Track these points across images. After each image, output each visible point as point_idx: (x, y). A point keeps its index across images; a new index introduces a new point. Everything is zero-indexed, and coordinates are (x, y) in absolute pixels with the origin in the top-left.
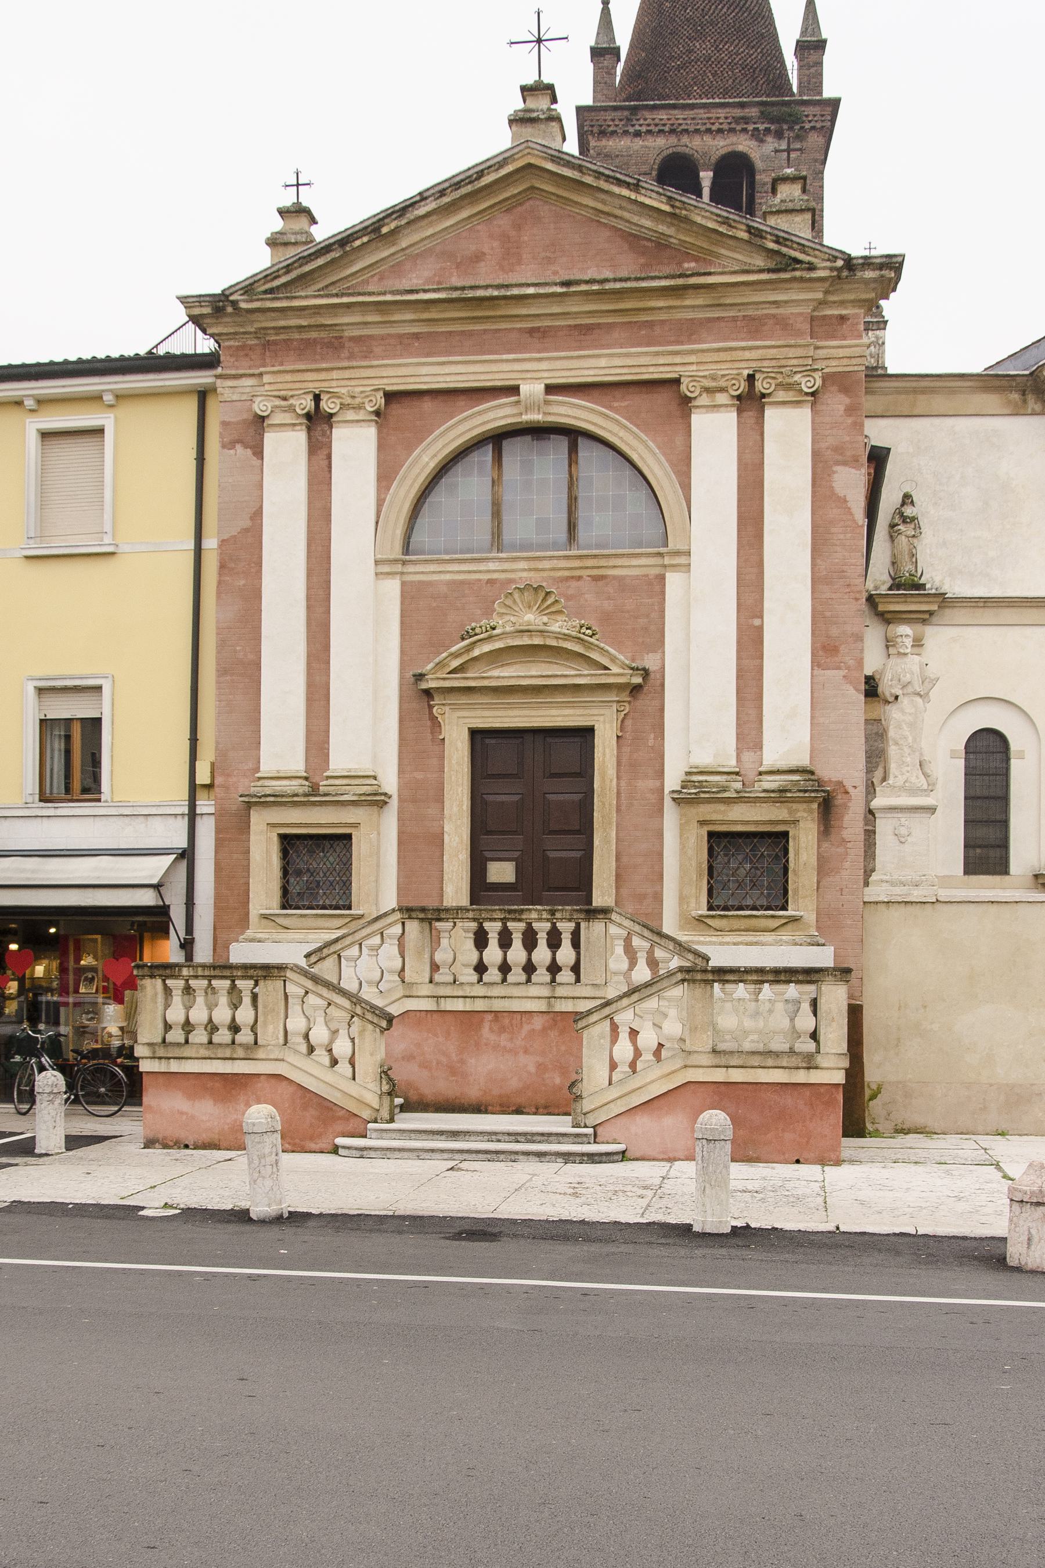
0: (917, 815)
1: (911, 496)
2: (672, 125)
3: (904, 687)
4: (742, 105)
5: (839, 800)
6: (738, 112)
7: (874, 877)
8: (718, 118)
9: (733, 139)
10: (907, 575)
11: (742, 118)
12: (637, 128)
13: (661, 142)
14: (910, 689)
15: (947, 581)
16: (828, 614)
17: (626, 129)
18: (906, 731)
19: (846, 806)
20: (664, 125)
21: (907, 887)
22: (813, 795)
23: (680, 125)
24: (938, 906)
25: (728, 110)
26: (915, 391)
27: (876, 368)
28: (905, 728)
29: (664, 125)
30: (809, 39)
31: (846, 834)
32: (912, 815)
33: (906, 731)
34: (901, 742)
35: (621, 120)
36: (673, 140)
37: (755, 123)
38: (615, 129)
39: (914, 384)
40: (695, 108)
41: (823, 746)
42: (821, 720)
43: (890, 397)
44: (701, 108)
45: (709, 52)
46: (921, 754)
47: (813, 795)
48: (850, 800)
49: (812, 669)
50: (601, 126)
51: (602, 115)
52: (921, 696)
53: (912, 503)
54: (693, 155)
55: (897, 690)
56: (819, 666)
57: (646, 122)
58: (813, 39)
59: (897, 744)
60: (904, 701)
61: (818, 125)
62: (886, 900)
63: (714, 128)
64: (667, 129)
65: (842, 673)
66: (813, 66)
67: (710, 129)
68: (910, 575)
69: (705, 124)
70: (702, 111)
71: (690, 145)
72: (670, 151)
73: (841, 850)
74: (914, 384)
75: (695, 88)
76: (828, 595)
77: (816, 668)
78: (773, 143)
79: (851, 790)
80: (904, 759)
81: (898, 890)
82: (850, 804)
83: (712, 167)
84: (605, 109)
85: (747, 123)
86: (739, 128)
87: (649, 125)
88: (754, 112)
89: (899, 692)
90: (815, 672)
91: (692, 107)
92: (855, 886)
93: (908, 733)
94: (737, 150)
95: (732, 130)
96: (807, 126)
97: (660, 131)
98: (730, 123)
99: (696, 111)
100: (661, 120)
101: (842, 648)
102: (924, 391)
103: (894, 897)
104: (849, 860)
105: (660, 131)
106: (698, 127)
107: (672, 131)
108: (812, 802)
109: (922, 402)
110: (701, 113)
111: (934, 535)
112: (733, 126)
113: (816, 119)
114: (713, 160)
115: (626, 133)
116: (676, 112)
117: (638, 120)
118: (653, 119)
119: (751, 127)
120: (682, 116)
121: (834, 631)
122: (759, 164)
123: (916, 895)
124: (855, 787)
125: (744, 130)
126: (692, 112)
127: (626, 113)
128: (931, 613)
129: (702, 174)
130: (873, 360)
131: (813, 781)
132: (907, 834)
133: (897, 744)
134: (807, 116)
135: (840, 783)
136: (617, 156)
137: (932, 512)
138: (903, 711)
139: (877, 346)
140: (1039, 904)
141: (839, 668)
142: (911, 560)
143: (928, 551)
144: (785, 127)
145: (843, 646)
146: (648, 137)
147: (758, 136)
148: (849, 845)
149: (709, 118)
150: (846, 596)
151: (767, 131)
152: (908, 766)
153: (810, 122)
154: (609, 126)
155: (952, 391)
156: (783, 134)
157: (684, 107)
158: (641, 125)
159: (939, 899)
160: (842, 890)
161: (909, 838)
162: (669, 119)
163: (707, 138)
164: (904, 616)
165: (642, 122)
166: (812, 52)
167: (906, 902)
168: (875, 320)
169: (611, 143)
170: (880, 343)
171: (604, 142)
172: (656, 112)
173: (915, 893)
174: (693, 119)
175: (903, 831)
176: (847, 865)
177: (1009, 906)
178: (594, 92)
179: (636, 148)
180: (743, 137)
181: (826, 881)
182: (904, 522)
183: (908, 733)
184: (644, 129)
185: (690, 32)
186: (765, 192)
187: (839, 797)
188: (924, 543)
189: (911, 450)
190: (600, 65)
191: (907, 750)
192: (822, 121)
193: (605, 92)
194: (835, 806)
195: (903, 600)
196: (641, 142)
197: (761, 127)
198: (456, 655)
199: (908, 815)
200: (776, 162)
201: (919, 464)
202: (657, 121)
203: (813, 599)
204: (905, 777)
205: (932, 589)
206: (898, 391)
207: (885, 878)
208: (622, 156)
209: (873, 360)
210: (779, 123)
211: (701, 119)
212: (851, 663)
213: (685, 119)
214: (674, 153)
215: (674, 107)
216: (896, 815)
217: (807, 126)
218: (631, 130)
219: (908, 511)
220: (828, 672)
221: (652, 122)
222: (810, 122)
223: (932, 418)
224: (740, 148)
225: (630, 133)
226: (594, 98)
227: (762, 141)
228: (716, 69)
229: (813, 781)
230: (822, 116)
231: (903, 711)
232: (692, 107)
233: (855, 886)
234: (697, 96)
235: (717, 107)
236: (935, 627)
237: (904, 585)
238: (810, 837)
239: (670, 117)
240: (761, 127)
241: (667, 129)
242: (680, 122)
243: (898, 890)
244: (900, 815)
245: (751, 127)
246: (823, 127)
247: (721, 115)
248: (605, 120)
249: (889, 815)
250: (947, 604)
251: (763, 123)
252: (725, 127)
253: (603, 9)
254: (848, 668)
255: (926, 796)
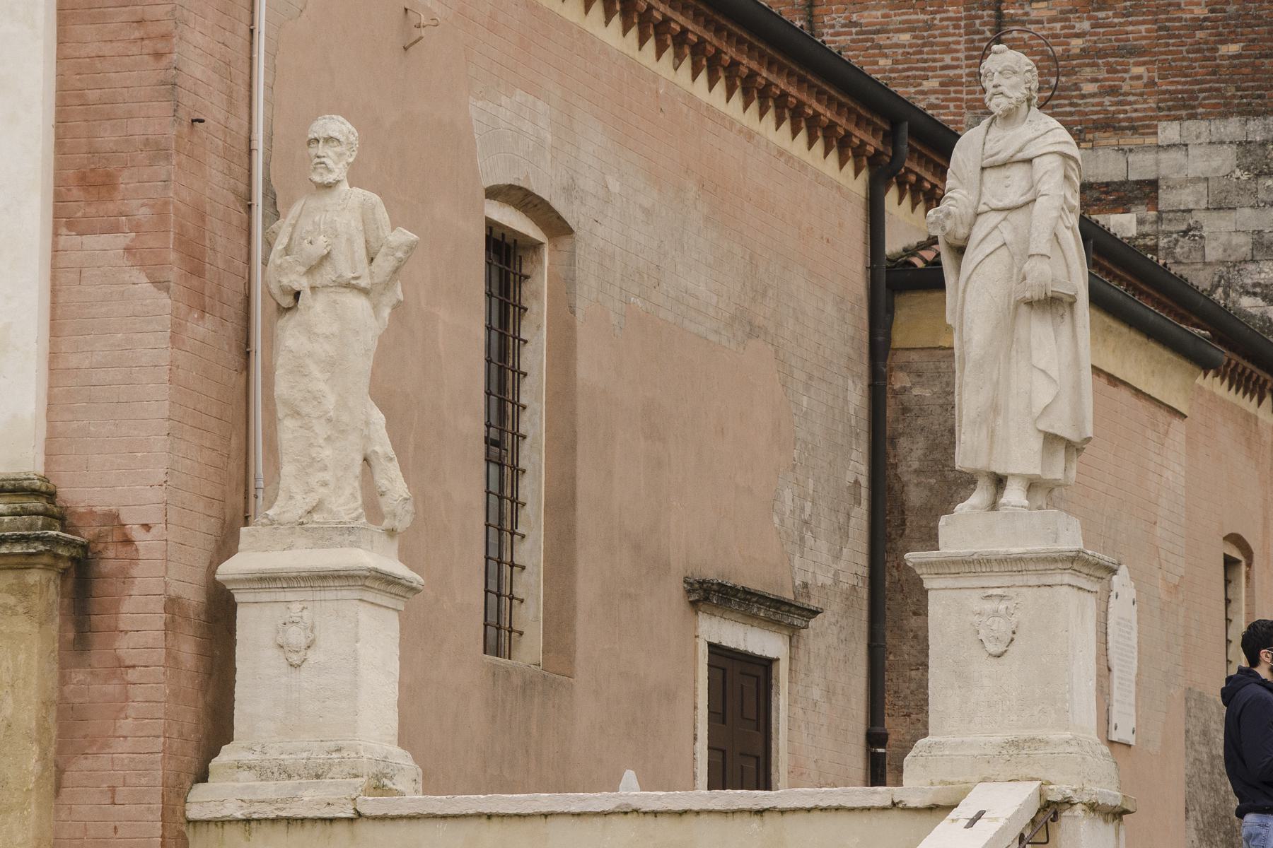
0: (330, 595)
3: (311, 270)
5: (111, 560)
7: (227, 755)
14: (327, 275)
16: (92, 95)
18: (319, 381)
19: (125, 576)
21: (294, 782)
22: (18, 549)
24: (362, 828)
28: (319, 375)
31: (126, 647)
32: (319, 595)
33: (319, 381)
34: (306, 409)
41: (75, 425)
42: (74, 361)
46: (367, 439)
47: (18, 549)
48: (135, 560)
49: (56, 234)
52: (365, 292)
55: (293, 277)
56: (70, 225)
59: (296, 413)
60: (316, 308)
62: (239, 815)
65: (122, 240)
73: (113, 688)
76: (92, 49)
77: (64, 231)
79: (137, 534)
80: (314, 453)
81: (270, 789)
82: (134, 572)
89: (302, 283)
90: (62, 239)
92: (144, 781)
93: (322, 386)
101: (126, 181)
103: (256, 807)
104: (131, 712)
108: (28, 567)
121: (107, 138)
123: (310, 800)
124: (147, 527)
131: (31, 513)
132: (303, 642)
133: (296, 413)
135: (113, 519)
138: (310, 333)
140: (599, 821)
141: (114, 229)
145: (126, 173)
148: (132, 675)
150: (134, 49)
152: (325, 468)
159: (362, 810)
160: (113, 789)
161: (310, 652)
167: (290, 821)
173: (308, 795)
175: (296, 636)
176: (126, 725)
177: (528, 825)
181: (78, 769)
183: (322, 386)
187: (110, 553)
191: (321, 429)
194: (103, 576)
198: (1126, 112)
199: (307, 595)
203: (61, 58)
204: (312, 500)
207: (246, 757)
212: (143, 214)
216: (281, 596)
220: (90, 241)
229: (31, 513)
231: (310, 333)
233: (144, 781)
238: (22, 657)
243: (270, 789)
244: (290, 596)
249: (264, 597)
254: (137, 229)
255: (352, 544)
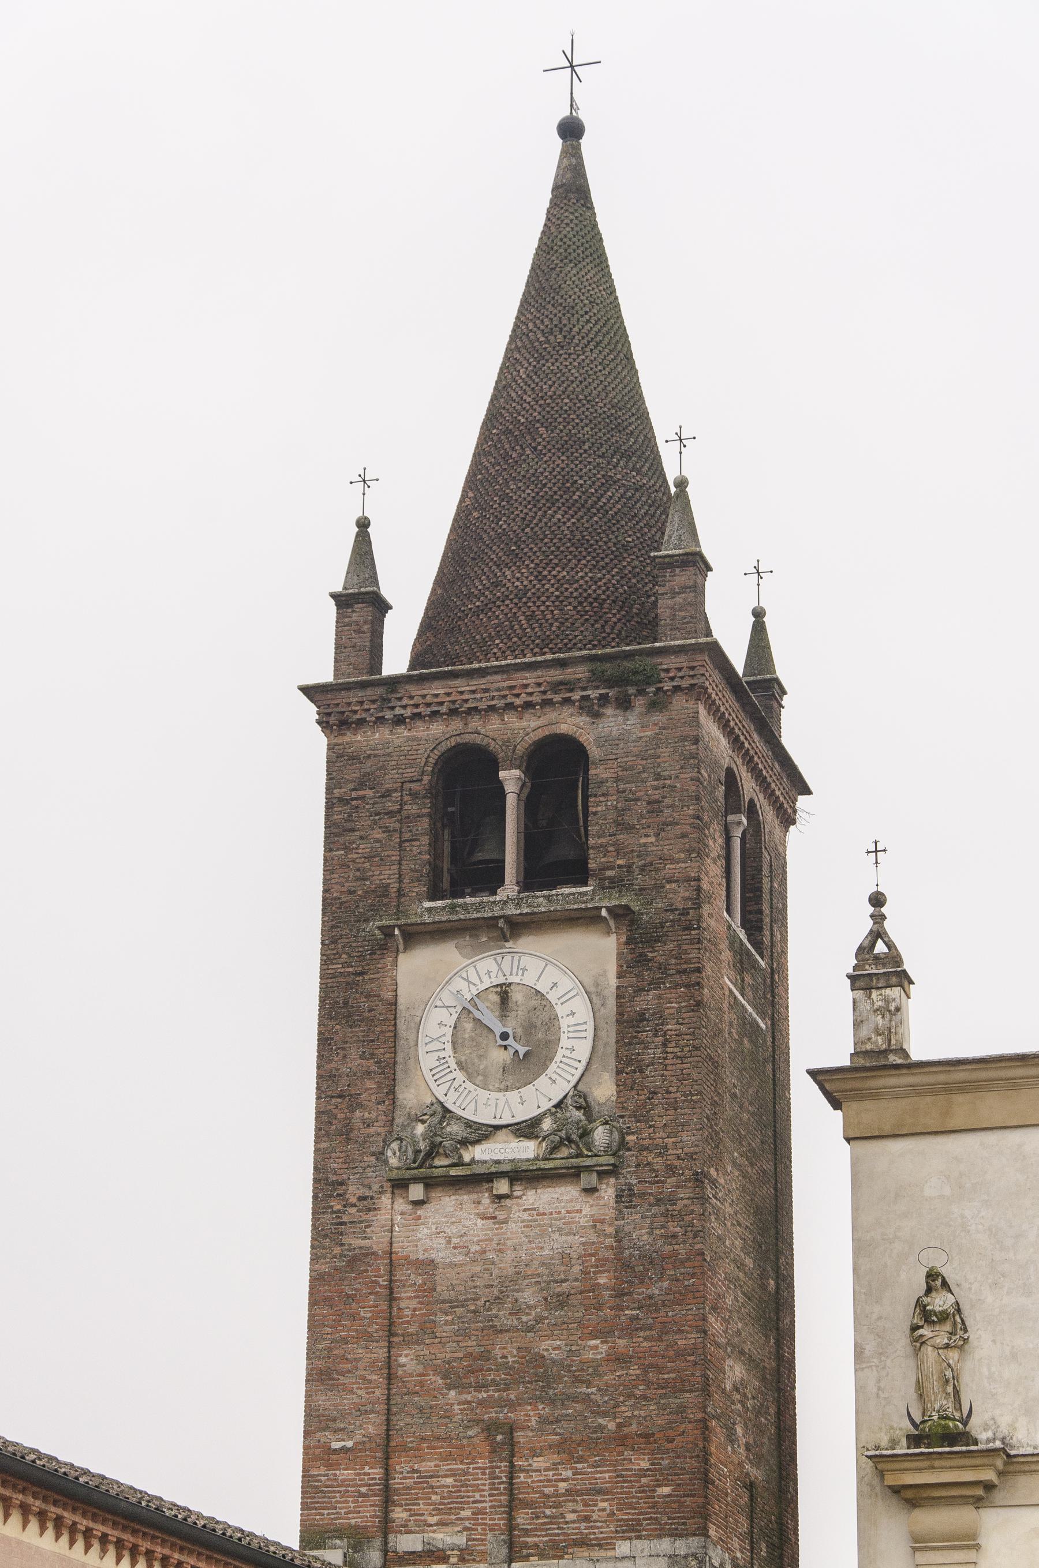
1: (938, 1274)
2: (454, 702)
4: (562, 664)
6: (556, 675)
8: (526, 686)
9: (551, 715)
10: (935, 1418)
11: (561, 683)
12: (398, 711)
13: (437, 729)
15: (1022, 1423)
17: (381, 714)
20: (441, 704)
23: (466, 701)
25: (539, 673)
26: (947, 1089)
27: (884, 1053)
29: (441, 704)
30: (670, 552)
35: (373, 702)
36: (456, 725)
37: (584, 689)
38: (364, 715)
39: (942, 1078)
40: (488, 674)
43: (904, 1102)
44: (496, 673)
45: (525, 583)
50: (343, 713)
51: (344, 697)
53: (945, 1284)
54: (488, 744)
57: (412, 702)
58: (677, 552)
61: (685, 683)
63: (518, 701)
64: (444, 709)
66: (679, 593)
67: (512, 703)
68: (941, 1418)
69: (505, 696)
70: (498, 677)
71: (482, 731)
72: (453, 742)
74: (942, 1078)
75: (497, 641)
78: (614, 716)
83: (518, 762)
84: (347, 687)
85: (571, 690)
86: (557, 698)
87: (416, 706)
88: (581, 672)
91: (483, 672)
94: (558, 732)
95: (547, 703)
96: (667, 686)
97: (435, 714)
98: (544, 692)
99: (489, 678)
100: (436, 696)
102: (963, 1088)
105: (435, 714)
106: (493, 703)
107: (453, 712)
109: (962, 1108)
110: (497, 681)
111: (994, 1341)
112: (549, 696)
113: (680, 674)
114: (520, 750)
115: (381, 720)
116: (457, 682)
117: (400, 699)
118: (424, 696)
119: (576, 696)
120: (468, 688)
122: (594, 752)
125: (567, 701)
126: (483, 681)
127: (380, 691)
128: (989, 1487)
129: (502, 774)
130: (880, 1040)
134: (667, 671)
136: (369, 756)
137: (990, 1299)
139: (887, 1015)
142: (944, 1390)
143: (985, 1370)
144: (631, 690)
146: (419, 723)
147: (592, 710)
149: (511, 688)
151: (604, 699)
153: (672, 679)
154: (355, 712)
155: (1014, 1085)
156: (630, 702)
157: (470, 674)
158: (404, 707)
162: (448, 694)
163: (510, 718)
164: (937, 1493)
165: (405, 702)
166: (677, 570)
168: (882, 971)
169: (359, 738)
170: (892, 1008)
171: (348, 737)
172: (428, 685)
174: (487, 690)
178: (336, 661)
179: (397, 742)
180: (567, 711)
182: (928, 1321)
184: (408, 712)
185: (500, 554)
186: (603, 795)
188: (977, 1357)
189: (947, 1191)
190: (347, 620)
192: (692, 676)
193: (352, 660)
195: (926, 1464)
196: (406, 733)
197: (593, 694)
198: (594, 1533)
200: (621, 746)
201: (963, 1216)
202: (429, 699)
205: (994, 1440)
206: (919, 1091)
208: (375, 756)
209: (880, 1040)
210: (621, 686)
211: (498, 690)
213: (473, 692)
214: (458, 745)
215: (454, 675)
217: (667, 686)
218: (389, 715)
219: (940, 1302)
221: (421, 701)
222: (672, 679)
223: (982, 1134)
224: (564, 729)
225: (387, 720)
226: (336, 670)
227: (597, 715)
228: (535, 609)
230: (693, 668)
232: (483, 672)
234: (499, 654)
235: (523, 669)
236: (999, 1510)
237: (928, 1436)
239: (450, 691)
240: (593, 694)
241: (444, 709)
242: (465, 697)
245: (576, 696)
246: (693, 685)
247: (529, 681)
248: (349, 704)
250: (1018, 1468)
251: (597, 688)
252: (536, 698)
253: (358, 535)
